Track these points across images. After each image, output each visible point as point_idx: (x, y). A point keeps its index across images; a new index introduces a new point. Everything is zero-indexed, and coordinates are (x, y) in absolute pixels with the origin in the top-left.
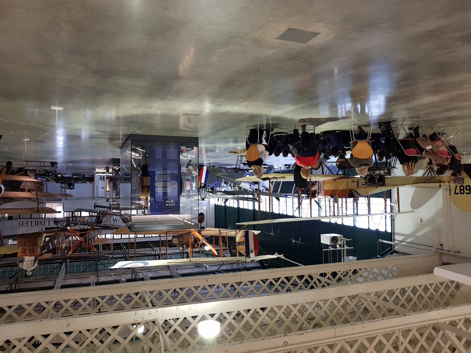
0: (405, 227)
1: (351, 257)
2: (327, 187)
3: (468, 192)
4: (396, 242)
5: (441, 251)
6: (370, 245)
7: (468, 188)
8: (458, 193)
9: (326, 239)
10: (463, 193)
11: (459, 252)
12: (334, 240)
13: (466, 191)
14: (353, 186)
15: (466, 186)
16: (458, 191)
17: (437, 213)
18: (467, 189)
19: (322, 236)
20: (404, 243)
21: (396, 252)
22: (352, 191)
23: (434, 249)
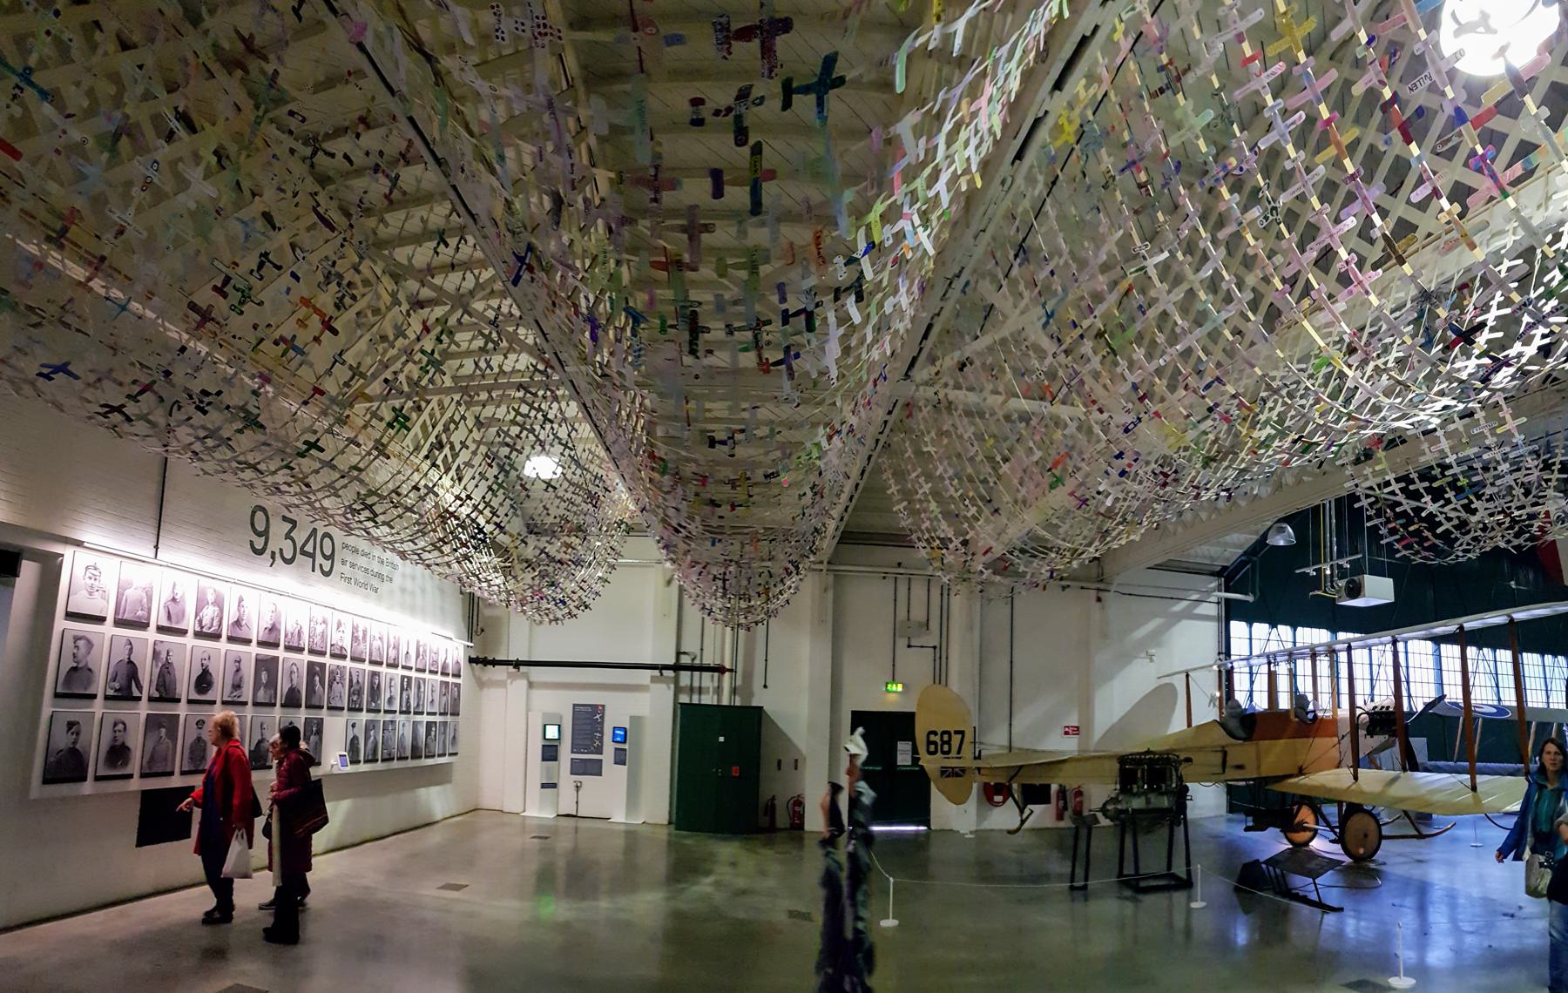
0: (1190, 641)
1: (1282, 543)
2: (1322, 744)
3: (932, 738)
4: (1214, 599)
5: (1101, 586)
6: (1270, 584)
7: (932, 748)
8: (957, 732)
9: (1378, 591)
10: (944, 733)
11: (1064, 588)
12: (1355, 591)
13: (937, 739)
14: (1242, 752)
15: (934, 753)
16: (956, 739)
17: (1111, 678)
18: (935, 743)
19: (1390, 598)
20: (1195, 597)
21: (1212, 574)
22: (1240, 733)
23: (1113, 588)
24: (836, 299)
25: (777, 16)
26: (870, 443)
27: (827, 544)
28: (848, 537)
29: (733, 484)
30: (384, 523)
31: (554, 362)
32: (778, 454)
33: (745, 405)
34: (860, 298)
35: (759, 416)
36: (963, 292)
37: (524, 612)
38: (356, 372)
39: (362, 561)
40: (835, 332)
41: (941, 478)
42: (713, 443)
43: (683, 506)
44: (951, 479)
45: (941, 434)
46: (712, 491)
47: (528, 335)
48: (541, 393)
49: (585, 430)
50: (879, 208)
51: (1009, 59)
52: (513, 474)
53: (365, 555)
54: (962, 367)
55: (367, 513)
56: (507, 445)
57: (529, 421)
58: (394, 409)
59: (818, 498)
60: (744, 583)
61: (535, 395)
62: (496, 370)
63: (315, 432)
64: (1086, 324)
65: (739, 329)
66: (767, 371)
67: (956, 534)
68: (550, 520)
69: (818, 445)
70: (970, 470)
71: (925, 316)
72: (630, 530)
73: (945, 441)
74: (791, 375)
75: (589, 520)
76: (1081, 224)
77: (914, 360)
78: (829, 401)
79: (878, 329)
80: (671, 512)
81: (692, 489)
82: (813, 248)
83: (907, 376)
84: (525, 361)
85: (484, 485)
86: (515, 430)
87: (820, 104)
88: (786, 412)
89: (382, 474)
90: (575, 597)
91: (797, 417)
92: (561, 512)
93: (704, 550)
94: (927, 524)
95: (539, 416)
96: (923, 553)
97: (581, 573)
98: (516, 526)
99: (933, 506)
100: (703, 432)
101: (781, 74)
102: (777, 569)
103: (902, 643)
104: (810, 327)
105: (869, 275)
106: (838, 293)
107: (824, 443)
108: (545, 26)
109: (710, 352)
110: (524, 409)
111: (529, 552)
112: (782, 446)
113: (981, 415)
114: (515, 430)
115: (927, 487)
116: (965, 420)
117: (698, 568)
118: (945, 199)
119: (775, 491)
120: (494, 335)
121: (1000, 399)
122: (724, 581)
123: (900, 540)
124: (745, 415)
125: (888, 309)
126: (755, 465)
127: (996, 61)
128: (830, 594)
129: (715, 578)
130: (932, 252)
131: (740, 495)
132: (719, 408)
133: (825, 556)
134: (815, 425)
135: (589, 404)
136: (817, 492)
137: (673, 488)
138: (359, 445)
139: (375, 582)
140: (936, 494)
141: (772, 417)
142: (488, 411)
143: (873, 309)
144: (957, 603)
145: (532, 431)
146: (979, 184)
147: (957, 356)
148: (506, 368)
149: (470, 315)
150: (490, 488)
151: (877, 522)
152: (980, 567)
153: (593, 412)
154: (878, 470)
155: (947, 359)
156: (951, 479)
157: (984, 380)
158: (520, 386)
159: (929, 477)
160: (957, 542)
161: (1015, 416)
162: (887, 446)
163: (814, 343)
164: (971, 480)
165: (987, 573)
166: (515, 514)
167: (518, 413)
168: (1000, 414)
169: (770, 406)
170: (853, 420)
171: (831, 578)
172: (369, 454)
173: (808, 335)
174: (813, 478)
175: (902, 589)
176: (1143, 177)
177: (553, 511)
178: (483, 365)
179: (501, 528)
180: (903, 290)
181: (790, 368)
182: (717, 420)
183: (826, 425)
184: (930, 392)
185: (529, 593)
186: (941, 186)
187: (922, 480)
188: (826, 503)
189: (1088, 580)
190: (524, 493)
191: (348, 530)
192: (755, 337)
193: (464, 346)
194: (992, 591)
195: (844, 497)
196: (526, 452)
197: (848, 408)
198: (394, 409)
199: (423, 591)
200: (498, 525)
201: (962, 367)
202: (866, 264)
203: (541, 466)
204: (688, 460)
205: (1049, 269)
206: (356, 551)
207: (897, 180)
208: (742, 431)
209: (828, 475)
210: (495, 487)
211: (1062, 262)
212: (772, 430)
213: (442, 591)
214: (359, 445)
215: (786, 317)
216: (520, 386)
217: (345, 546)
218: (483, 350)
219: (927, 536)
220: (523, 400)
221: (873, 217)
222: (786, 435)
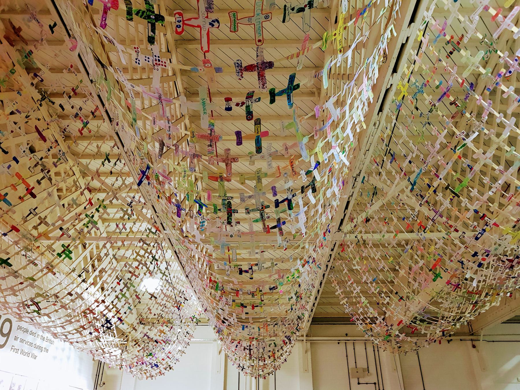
11: (449, 341)
23: (481, 338)
24: (302, 192)
25: (265, 61)
26: (323, 267)
27: (305, 325)
28: (316, 321)
29: (253, 294)
30: (45, 315)
31: (161, 228)
32: (276, 276)
33: (257, 251)
34: (314, 190)
35: (265, 257)
36: (363, 182)
37: (131, 372)
38: (43, 221)
39: (30, 338)
40: (303, 209)
41: (366, 283)
42: (241, 272)
43: (226, 308)
44: (371, 283)
45: (362, 258)
46: (242, 298)
47: (148, 213)
48: (152, 244)
49: (175, 266)
50: (320, 144)
51: (373, 63)
52: (132, 289)
53: (32, 333)
54: (367, 220)
55: (34, 308)
56: (130, 272)
57: (144, 260)
58: (63, 246)
59: (299, 299)
60: (261, 350)
61: (149, 245)
62: (128, 230)
63: (8, 253)
64: (435, 184)
65: (253, 210)
66: (268, 232)
67: (379, 314)
68: (151, 316)
69: (297, 270)
70: (381, 277)
71: (346, 197)
72: (198, 322)
73: (365, 262)
74: (281, 233)
75: (175, 316)
76: (420, 134)
77: (342, 221)
78: (301, 246)
79: (324, 206)
80: (220, 311)
81: (231, 297)
82: (290, 167)
83: (339, 229)
84: (145, 225)
85: (114, 295)
86: (136, 264)
87: (289, 98)
88: (278, 254)
89: (51, 283)
90: (164, 362)
91: (284, 256)
92: (159, 311)
93: (238, 333)
94: (361, 310)
95: (150, 257)
96: (361, 327)
97: (168, 348)
98: (132, 319)
99: (363, 299)
100: (236, 266)
101: (269, 86)
102: (279, 342)
103: (354, 381)
104: (290, 207)
105: (318, 178)
106: (303, 190)
107: (301, 269)
108: (159, 61)
109: (239, 223)
110: (142, 252)
111: (138, 335)
112: (278, 272)
113: (384, 246)
114: (136, 264)
115: (358, 289)
116: (375, 249)
117: (236, 343)
118: (351, 136)
119: (276, 297)
120: (129, 212)
121: (392, 235)
122: (250, 350)
123: (346, 320)
124: (258, 256)
125: (329, 194)
126: (264, 283)
127: (368, 65)
128: (309, 353)
129: (245, 349)
130: (347, 163)
131: (256, 300)
132: (244, 253)
133: (304, 332)
134: (295, 259)
135: (177, 252)
136: (299, 296)
137: (221, 297)
138: (36, 265)
139: (36, 352)
140: (364, 292)
141: (272, 257)
142: (121, 252)
143: (321, 196)
144: (385, 356)
145: (146, 264)
146: (365, 127)
147: (364, 215)
148: (135, 229)
149: (117, 199)
150: (117, 297)
151: (331, 311)
152: (397, 333)
153: (179, 256)
154: (329, 282)
155: (359, 217)
156: (371, 283)
157: (381, 225)
158: (141, 240)
159: (358, 282)
160: (380, 319)
161: (403, 243)
162: (332, 268)
163: (293, 215)
164: (383, 282)
165: (402, 336)
166: (131, 312)
167: (138, 254)
168: (394, 243)
169: (271, 251)
170: (314, 255)
171: (309, 344)
172: (42, 271)
173: (289, 212)
174: (296, 288)
175: (350, 347)
176: (452, 99)
177: (154, 311)
178: (121, 226)
179: (121, 321)
180: (335, 184)
181: (281, 230)
182: (244, 259)
183: (301, 259)
184: (353, 236)
185: (135, 360)
186: (348, 131)
187: (355, 285)
188: (303, 302)
189: (464, 334)
190: (138, 300)
191: (20, 318)
192: (261, 215)
193: (111, 216)
194: (406, 347)
195: (312, 298)
196: (140, 277)
197: (311, 248)
198: (63, 246)
199: (68, 358)
200: (120, 319)
201: (367, 220)
202: (316, 173)
203: (150, 284)
204: (229, 282)
205: (407, 161)
206: (27, 331)
207: (328, 131)
208: (257, 265)
209: (303, 286)
210: (120, 296)
211: (414, 156)
212: (272, 263)
213: (81, 359)
214: (36, 265)
215: (277, 204)
216: (141, 240)
217: (19, 328)
218: (122, 218)
219: (362, 317)
220: (142, 248)
221: (318, 149)
222: (281, 266)
